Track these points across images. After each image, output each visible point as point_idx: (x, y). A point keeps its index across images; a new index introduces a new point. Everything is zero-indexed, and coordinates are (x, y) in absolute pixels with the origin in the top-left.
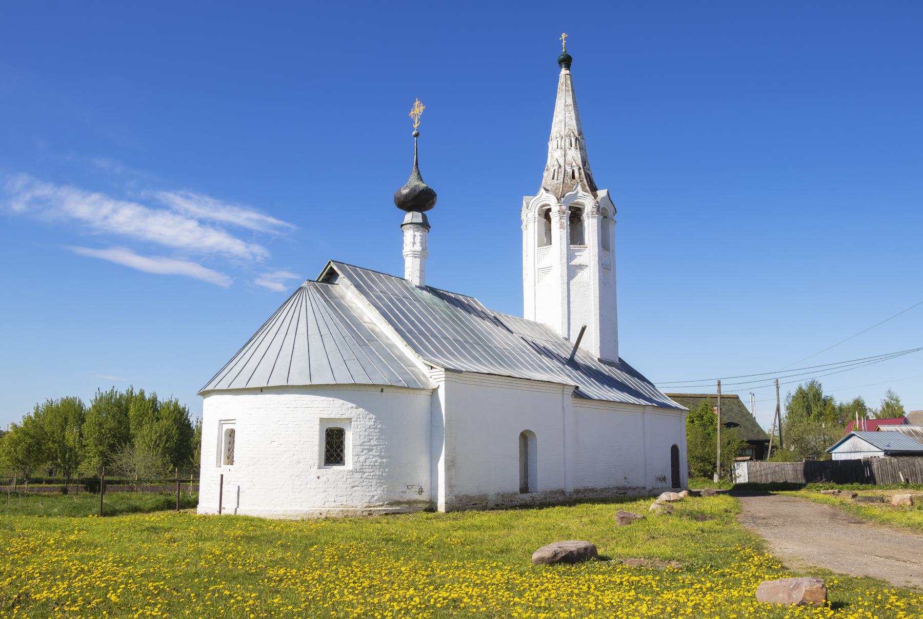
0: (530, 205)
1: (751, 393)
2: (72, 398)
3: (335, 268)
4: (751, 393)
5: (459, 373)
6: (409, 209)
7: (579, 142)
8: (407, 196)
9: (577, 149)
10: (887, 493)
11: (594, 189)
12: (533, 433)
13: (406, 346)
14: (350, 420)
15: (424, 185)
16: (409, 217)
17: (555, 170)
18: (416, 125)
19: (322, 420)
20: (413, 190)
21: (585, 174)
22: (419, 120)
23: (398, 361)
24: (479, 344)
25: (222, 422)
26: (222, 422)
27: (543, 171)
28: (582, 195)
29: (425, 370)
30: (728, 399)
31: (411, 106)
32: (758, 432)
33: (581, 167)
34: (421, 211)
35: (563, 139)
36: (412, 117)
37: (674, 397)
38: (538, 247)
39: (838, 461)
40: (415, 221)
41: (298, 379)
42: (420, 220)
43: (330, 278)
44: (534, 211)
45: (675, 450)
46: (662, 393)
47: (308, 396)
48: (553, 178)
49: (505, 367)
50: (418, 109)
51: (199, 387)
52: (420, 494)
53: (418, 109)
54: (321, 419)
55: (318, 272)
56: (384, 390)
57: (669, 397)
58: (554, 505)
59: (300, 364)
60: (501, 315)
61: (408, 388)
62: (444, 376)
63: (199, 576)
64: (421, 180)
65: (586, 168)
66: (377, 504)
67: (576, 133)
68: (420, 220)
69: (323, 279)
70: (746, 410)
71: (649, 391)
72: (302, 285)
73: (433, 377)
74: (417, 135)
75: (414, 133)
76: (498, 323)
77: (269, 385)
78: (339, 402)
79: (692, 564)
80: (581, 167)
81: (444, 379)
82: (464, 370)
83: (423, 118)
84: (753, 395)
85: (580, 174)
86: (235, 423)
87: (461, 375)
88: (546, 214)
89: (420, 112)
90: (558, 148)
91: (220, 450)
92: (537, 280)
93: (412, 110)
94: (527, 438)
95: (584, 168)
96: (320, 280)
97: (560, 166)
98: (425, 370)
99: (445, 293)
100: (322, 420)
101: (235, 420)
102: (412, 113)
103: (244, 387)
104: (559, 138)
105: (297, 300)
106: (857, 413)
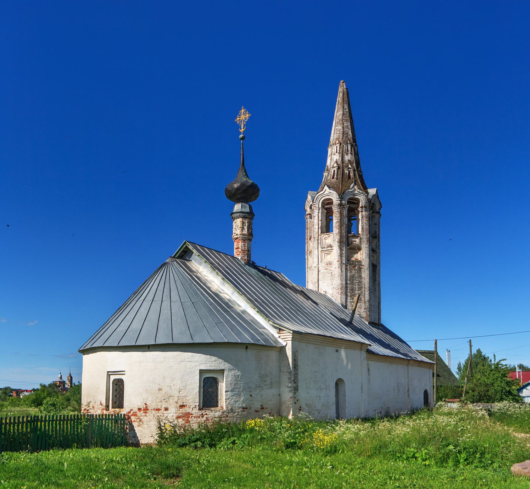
0: (315, 200)
1: (447, 350)
2: (52, 383)
3: (190, 247)
4: (447, 350)
5: (301, 334)
6: (238, 201)
7: (354, 149)
8: (238, 189)
9: (352, 154)
10: (336, 230)
11: (365, 189)
12: (343, 380)
13: (257, 312)
14: (222, 371)
15: (250, 181)
16: (237, 207)
17: (334, 171)
18: (242, 130)
19: (202, 372)
20: (243, 185)
21: (358, 175)
22: (244, 125)
23: (252, 324)
24: (300, 311)
25: (109, 373)
26: (109, 373)
27: (324, 171)
28: (357, 193)
29: (274, 332)
30: (430, 354)
31: (237, 113)
32: (454, 380)
33: (356, 169)
34: (246, 202)
35: (342, 145)
36: (238, 123)
37: (423, 353)
38: (112, 408)
39: (332, 216)
40: (244, 210)
41: (161, 340)
42: (247, 210)
43: (184, 255)
44: (318, 204)
45: (426, 393)
46: (414, 350)
47: (199, 355)
48: (333, 178)
49: (328, 331)
50: (244, 116)
51: (80, 345)
52: (388, 407)
53: (244, 116)
54: (200, 370)
55: (177, 250)
56: (248, 347)
57: (419, 353)
58: (219, 370)
59: (150, 327)
60: (304, 289)
61: (265, 346)
62: (291, 336)
63: (425, 465)
64: (248, 177)
65: (359, 170)
66: (410, 383)
67: (352, 140)
68: (247, 210)
69: (178, 256)
70: (444, 363)
71: (398, 344)
72: (167, 261)
73: (281, 337)
74: (243, 138)
75: (241, 136)
76: (308, 299)
77: (136, 344)
78: (214, 358)
79: (451, 412)
80: (356, 169)
81: (291, 339)
82: (303, 332)
83: (248, 124)
84: (449, 351)
85: (355, 175)
86: (124, 374)
87: (302, 336)
88: (327, 205)
89: (246, 119)
90: (337, 152)
91: (108, 386)
92: (320, 260)
93: (238, 116)
94: (338, 384)
95: (357, 170)
96: (176, 257)
97: (339, 168)
98: (274, 332)
99: (320, 219)
100: (202, 372)
101: (125, 371)
102: (238, 119)
103: (134, 344)
104: (338, 144)
105: (168, 268)
106: (342, 88)
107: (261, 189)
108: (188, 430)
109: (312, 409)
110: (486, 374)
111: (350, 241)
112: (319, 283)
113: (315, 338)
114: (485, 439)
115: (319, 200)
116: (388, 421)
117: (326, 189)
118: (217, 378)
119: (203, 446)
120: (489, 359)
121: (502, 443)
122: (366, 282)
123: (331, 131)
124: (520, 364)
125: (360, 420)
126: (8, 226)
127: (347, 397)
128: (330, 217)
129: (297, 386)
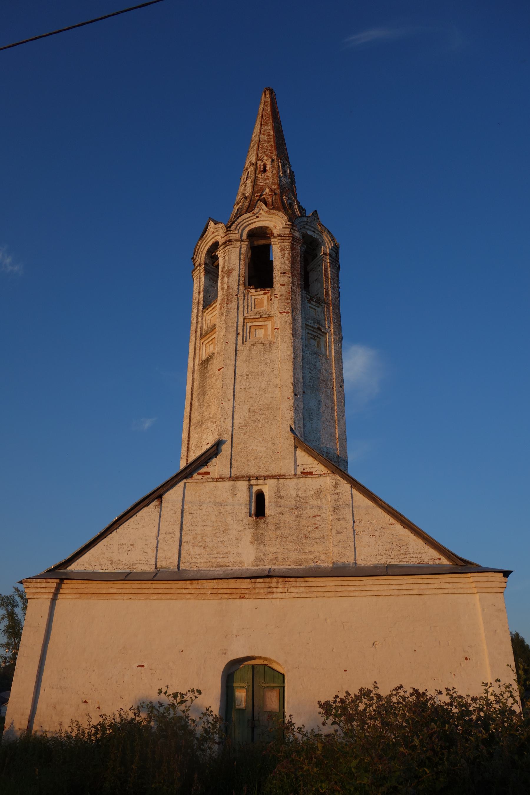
10: (266, 323)
60: (223, 278)
107: (289, 431)
108: (203, 750)
109: (222, 497)
110: (429, 718)
111: (223, 239)
112: (160, 524)
113: (206, 243)
114: (298, 503)
115: (242, 228)
116: (252, 535)
117: (217, 305)
118: (267, 228)
119: (223, 295)
120: (385, 562)
121: (391, 539)
122: (297, 208)
123: (191, 312)
124: (273, 89)
125: (429, 751)
126: (345, 671)
127: (238, 602)
128: (216, 264)
129: (149, 703)
